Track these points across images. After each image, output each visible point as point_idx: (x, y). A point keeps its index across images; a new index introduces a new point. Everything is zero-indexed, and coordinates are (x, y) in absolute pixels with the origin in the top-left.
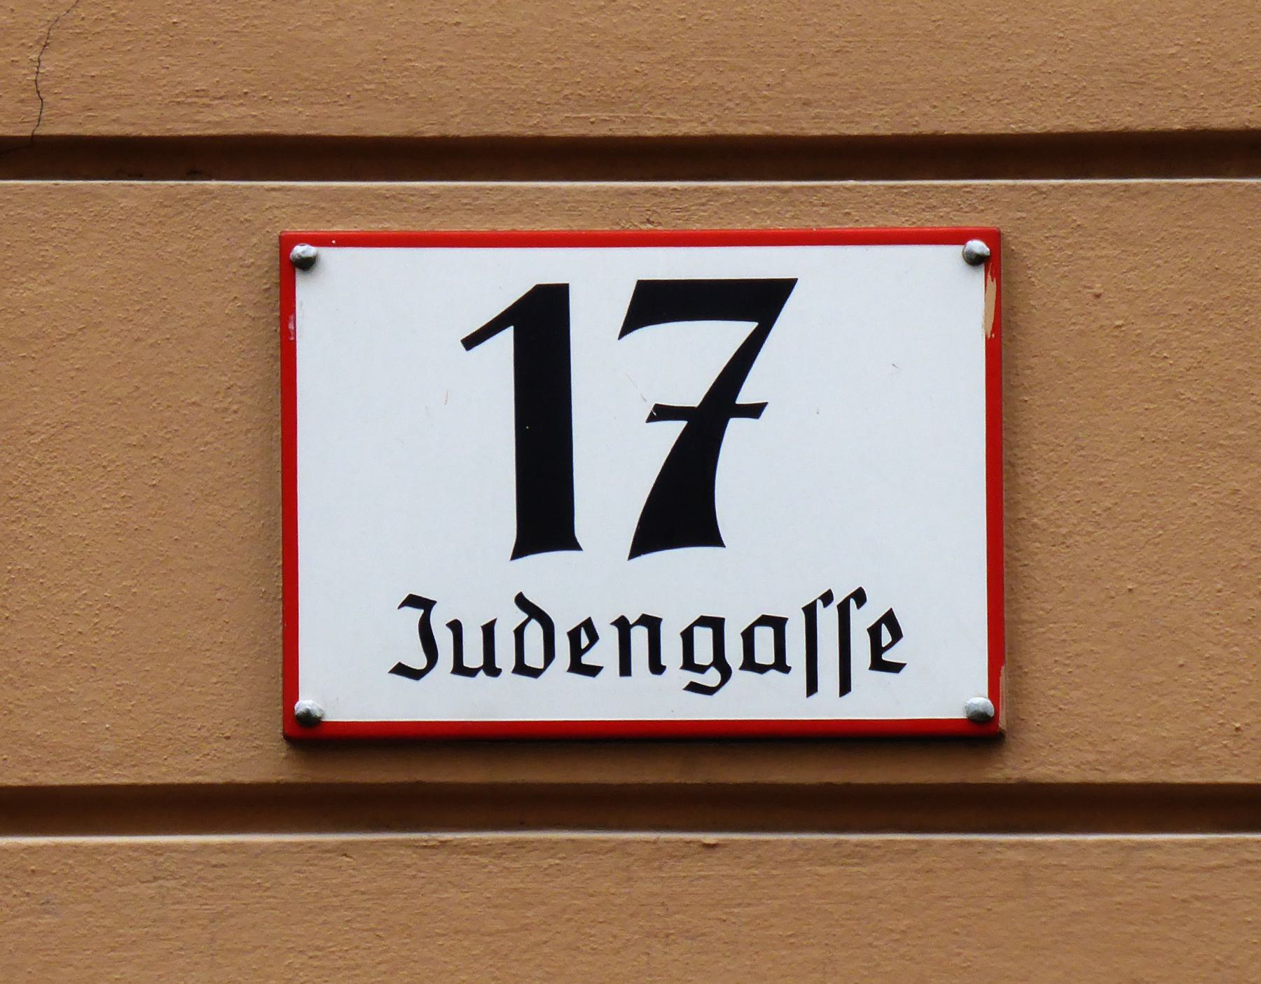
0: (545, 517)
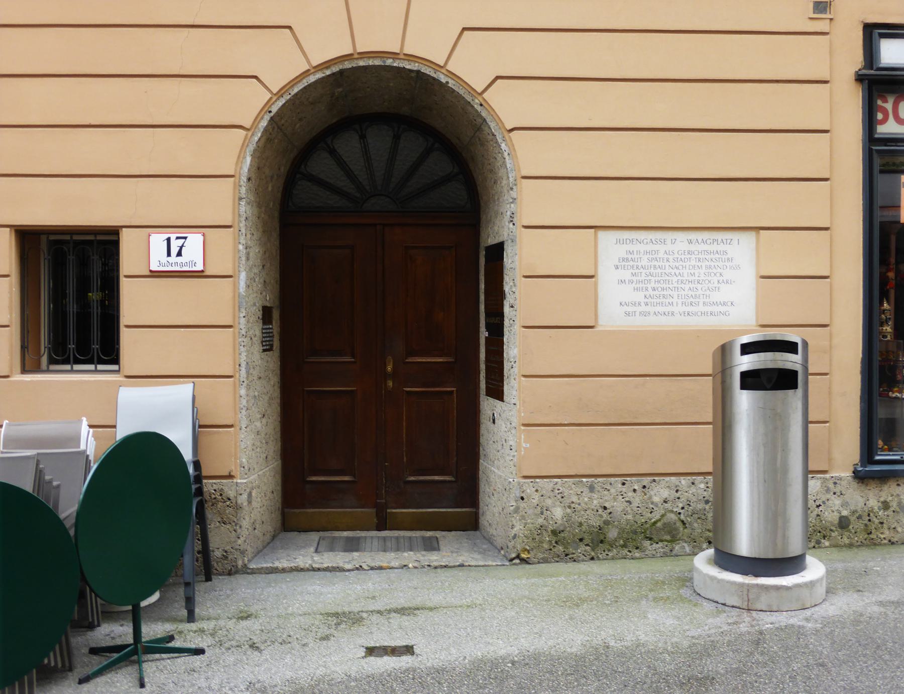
0: (169, 254)
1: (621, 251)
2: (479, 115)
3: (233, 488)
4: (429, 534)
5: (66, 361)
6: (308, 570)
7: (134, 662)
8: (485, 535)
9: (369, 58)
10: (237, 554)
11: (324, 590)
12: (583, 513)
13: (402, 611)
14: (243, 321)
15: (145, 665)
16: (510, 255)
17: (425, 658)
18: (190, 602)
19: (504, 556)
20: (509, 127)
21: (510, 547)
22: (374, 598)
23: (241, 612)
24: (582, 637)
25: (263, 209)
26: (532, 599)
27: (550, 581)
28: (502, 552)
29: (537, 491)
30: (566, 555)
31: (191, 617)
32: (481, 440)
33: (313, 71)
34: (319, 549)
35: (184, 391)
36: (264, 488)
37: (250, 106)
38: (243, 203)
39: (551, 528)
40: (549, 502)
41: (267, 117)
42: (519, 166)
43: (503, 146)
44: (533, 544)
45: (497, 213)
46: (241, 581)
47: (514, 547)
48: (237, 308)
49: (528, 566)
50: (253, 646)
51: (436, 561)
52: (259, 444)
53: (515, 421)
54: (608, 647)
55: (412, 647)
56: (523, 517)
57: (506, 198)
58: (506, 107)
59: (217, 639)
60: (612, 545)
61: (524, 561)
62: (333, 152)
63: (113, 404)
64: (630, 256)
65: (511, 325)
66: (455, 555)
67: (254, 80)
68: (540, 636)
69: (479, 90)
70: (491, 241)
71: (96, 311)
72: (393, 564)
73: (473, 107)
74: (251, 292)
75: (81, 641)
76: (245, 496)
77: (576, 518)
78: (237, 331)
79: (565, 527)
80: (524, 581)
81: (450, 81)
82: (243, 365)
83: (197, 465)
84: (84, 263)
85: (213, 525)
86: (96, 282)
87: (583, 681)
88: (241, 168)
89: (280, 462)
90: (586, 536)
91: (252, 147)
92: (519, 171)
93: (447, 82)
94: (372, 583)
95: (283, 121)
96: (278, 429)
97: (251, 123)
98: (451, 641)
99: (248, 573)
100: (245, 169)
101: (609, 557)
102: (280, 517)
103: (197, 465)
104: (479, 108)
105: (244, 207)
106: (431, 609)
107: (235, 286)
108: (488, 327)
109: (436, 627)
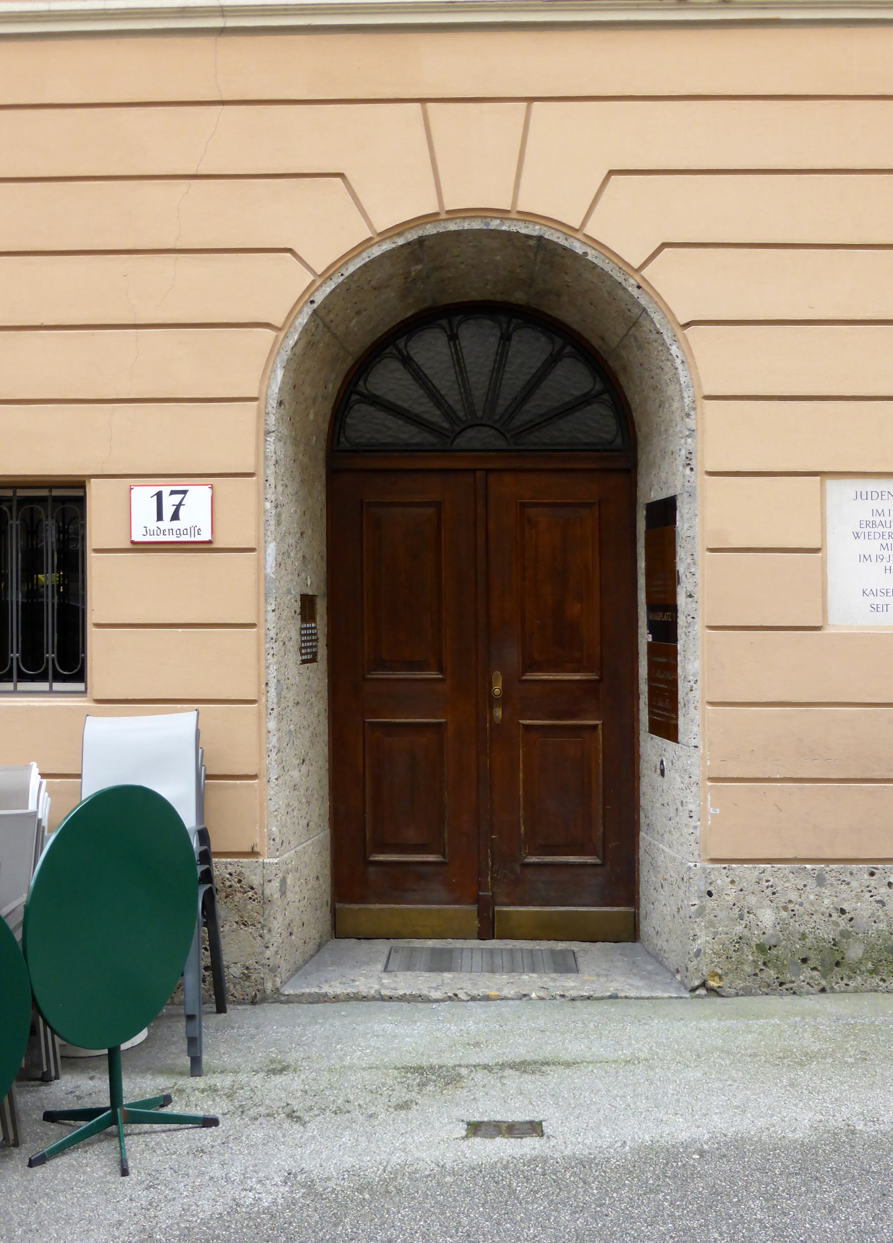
0: (160, 517)
1: (864, 510)
2: (636, 303)
3: (259, 871)
4: (561, 945)
5: (42, 677)
6: (374, 999)
7: (112, 1135)
8: (650, 949)
9: (464, 218)
10: (264, 972)
11: (400, 1031)
12: (806, 918)
13: (522, 1067)
14: (271, 617)
15: (128, 1141)
16: (686, 516)
17: (561, 1141)
18: (194, 1043)
19: (682, 983)
20: (682, 321)
21: (691, 969)
22: (477, 1044)
23: (272, 1061)
24: (810, 1115)
25: (302, 448)
26: (728, 1053)
27: (757, 1024)
28: (678, 977)
29: (732, 882)
30: (781, 984)
31: (196, 1068)
32: (643, 802)
33: (377, 239)
34: (390, 967)
35: (182, 724)
36: (305, 872)
37: (282, 294)
38: (271, 439)
39: (755, 941)
40: (752, 900)
41: (308, 310)
42: (699, 380)
43: (674, 349)
44: (727, 966)
45: (664, 452)
46: (270, 1012)
47: (697, 970)
48: (262, 598)
49: (719, 1000)
50: (292, 1115)
51: (573, 988)
52: (296, 804)
53: (697, 772)
54: (853, 1132)
55: (540, 1123)
56: (711, 924)
57: (678, 428)
58: (678, 290)
59: (237, 1104)
60: (854, 970)
61: (714, 992)
62: (407, 361)
63: (77, 743)
64: (877, 519)
65: (689, 625)
66: (603, 980)
67: (288, 255)
68: (744, 1111)
69: (636, 265)
70: (657, 495)
71: (51, 602)
72: (505, 992)
73: (625, 289)
74: (283, 572)
75: (32, 1101)
76: (276, 884)
77: (796, 927)
78: (262, 631)
79: (779, 941)
80: (714, 1024)
81: (589, 250)
82: (273, 683)
83: (203, 835)
84: (32, 530)
85: (227, 928)
86: (51, 557)
87: (815, 1185)
88: (268, 387)
89: (328, 831)
90: (812, 955)
91: (285, 355)
92: (700, 387)
93: (586, 254)
94: (475, 1021)
95: (332, 316)
96: (326, 781)
97: (283, 320)
98: (601, 1115)
99: (281, 1002)
100: (275, 388)
101: (850, 988)
102: (328, 916)
103: (203, 835)
104: (635, 292)
105: (272, 446)
106: (568, 1065)
107: (260, 565)
108: (652, 627)
109: (577, 1093)
